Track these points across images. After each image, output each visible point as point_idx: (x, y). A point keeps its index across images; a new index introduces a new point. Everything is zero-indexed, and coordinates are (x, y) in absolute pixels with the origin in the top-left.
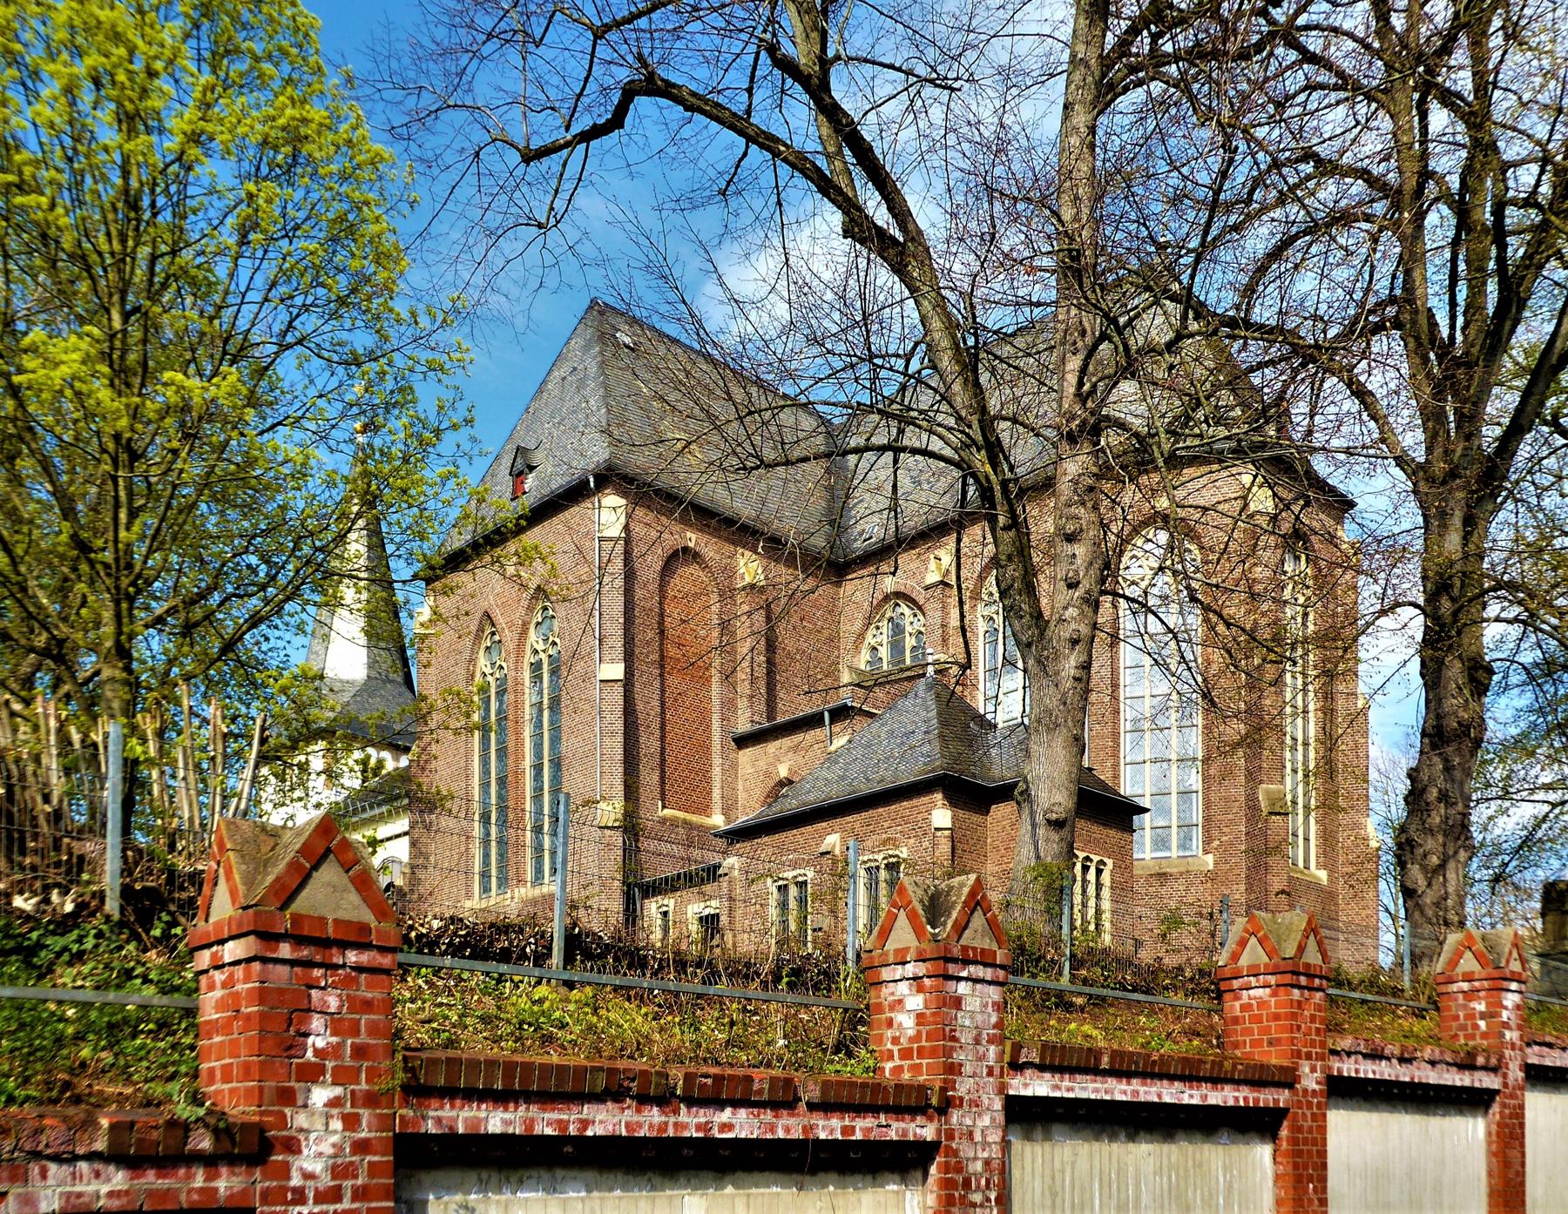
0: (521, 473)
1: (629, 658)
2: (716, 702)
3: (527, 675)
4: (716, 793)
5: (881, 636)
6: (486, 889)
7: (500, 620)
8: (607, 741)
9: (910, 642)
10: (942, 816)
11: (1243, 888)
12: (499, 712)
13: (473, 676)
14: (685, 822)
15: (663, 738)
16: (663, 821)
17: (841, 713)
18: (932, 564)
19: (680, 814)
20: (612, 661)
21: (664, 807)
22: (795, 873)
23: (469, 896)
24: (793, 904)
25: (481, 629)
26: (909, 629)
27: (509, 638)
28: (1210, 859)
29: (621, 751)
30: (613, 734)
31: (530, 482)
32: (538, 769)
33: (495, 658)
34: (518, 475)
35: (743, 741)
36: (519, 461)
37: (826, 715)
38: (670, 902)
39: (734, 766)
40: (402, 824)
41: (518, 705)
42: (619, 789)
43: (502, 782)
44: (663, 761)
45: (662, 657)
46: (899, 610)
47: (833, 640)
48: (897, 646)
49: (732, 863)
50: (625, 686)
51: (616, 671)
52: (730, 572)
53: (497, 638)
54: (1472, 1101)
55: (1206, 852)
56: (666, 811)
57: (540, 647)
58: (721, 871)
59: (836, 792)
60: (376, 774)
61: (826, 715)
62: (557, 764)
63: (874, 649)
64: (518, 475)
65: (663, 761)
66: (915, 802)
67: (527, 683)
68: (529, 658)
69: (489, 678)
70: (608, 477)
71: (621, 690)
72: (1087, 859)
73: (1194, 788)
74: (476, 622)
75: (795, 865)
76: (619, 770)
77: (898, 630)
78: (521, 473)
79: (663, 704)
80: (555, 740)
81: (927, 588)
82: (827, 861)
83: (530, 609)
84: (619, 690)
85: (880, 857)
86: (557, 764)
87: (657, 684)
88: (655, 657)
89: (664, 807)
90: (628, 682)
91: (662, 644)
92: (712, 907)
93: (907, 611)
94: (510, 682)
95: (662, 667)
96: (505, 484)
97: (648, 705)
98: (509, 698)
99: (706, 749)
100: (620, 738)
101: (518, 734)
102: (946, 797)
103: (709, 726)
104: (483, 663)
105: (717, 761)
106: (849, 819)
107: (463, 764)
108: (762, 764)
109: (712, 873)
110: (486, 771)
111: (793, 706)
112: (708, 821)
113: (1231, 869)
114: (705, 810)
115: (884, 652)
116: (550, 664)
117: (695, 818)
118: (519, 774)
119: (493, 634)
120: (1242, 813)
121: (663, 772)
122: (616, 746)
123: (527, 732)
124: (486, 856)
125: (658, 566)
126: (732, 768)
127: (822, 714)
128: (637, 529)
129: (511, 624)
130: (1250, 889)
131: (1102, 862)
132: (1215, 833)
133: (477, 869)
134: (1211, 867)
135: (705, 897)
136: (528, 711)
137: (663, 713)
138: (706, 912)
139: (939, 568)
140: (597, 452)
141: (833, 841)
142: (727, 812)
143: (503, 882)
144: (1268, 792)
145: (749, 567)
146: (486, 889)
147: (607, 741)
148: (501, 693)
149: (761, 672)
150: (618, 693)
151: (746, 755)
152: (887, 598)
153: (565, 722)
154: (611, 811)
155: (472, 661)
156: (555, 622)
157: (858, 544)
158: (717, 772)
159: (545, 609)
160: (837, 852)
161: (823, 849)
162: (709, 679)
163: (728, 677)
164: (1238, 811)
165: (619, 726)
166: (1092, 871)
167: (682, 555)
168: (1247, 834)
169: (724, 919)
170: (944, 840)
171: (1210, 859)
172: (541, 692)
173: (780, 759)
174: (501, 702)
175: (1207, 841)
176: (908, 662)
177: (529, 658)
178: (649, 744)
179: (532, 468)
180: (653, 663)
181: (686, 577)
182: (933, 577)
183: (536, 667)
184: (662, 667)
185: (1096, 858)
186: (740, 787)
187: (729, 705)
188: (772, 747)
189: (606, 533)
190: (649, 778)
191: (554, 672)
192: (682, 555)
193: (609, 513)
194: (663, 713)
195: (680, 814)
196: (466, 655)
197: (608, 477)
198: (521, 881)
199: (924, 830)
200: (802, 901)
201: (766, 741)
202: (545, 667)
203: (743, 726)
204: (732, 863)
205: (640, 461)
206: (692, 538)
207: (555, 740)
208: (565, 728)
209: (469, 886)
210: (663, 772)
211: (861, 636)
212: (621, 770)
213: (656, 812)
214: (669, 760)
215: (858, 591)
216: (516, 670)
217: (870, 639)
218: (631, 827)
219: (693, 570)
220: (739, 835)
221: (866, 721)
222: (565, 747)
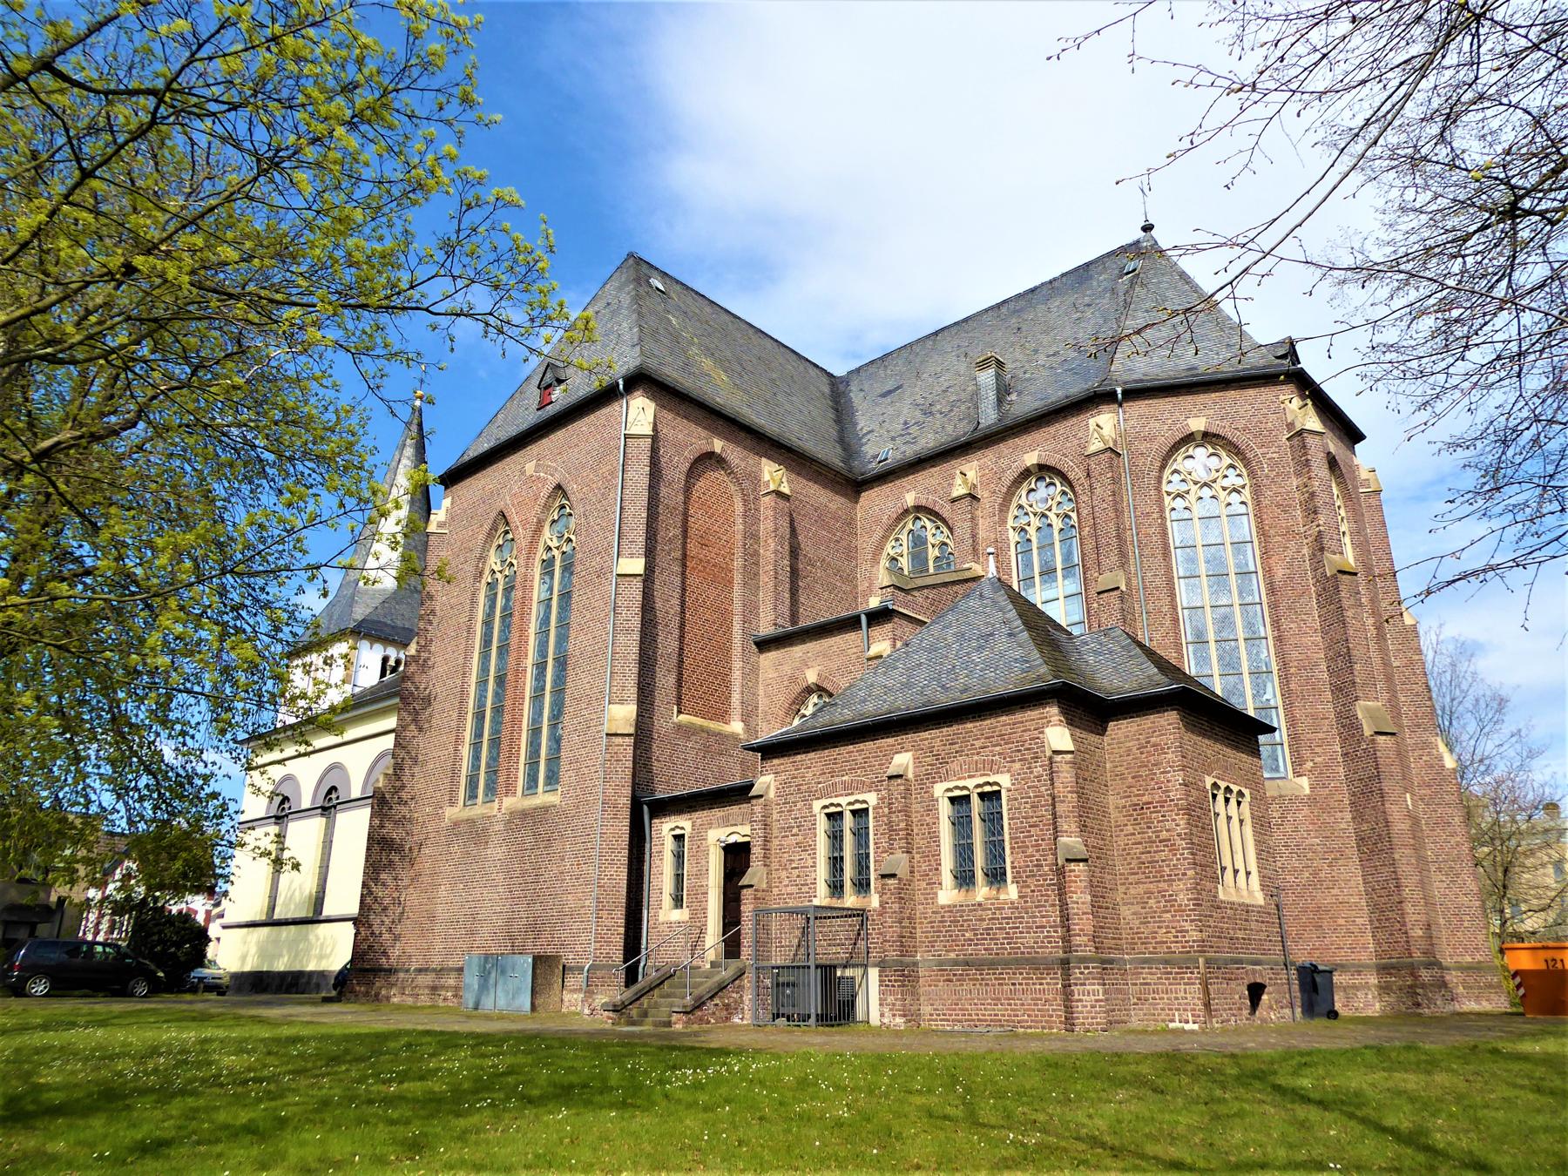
0: (549, 386)
1: (650, 553)
2: (737, 607)
3: (537, 571)
4: (736, 698)
5: (901, 547)
6: (472, 795)
7: (515, 519)
8: (621, 638)
9: (933, 553)
10: (1059, 736)
11: (1349, 816)
12: (504, 609)
13: (481, 573)
14: (702, 729)
15: (682, 637)
16: (679, 726)
17: (880, 616)
18: (959, 480)
19: (698, 721)
20: (632, 556)
21: (679, 712)
22: (851, 799)
23: (452, 803)
24: (848, 840)
25: (494, 528)
26: (931, 540)
27: (522, 535)
28: (1305, 782)
29: (636, 650)
30: (628, 631)
31: (557, 393)
32: (541, 667)
33: (506, 555)
34: (546, 388)
35: (764, 645)
36: (549, 375)
37: (863, 618)
38: (684, 823)
39: (755, 670)
40: (391, 722)
41: (526, 601)
42: (632, 691)
43: (501, 680)
44: (681, 662)
45: (685, 556)
46: (919, 524)
47: (851, 553)
48: (919, 558)
49: (767, 781)
50: (644, 581)
51: (637, 565)
52: (755, 479)
53: (510, 536)
54: (1060, 872)
55: (1298, 774)
56: (682, 717)
57: (555, 543)
58: (753, 792)
59: (904, 703)
60: (394, 670)
61: (863, 618)
62: (562, 663)
63: (894, 559)
64: (546, 388)
65: (681, 662)
66: (1019, 716)
67: (537, 577)
68: (541, 554)
69: (498, 575)
70: (639, 380)
71: (640, 585)
72: (1228, 790)
73: (1272, 703)
74: (490, 522)
75: (849, 789)
76: (633, 670)
77: (919, 542)
78: (549, 386)
79: (683, 603)
80: (562, 638)
81: (954, 501)
82: (898, 787)
83: (547, 507)
84: (638, 585)
85: (970, 783)
86: (562, 663)
87: (677, 581)
88: (678, 554)
89: (679, 712)
90: (648, 577)
91: (684, 544)
92: (739, 833)
93: (928, 524)
94: (519, 579)
95: (684, 566)
96: (533, 394)
97: (668, 605)
98: (517, 594)
99: (726, 651)
100: (636, 636)
101: (523, 630)
102: (1064, 712)
103: (730, 628)
104: (493, 561)
105: (737, 664)
106: (925, 735)
107: (461, 661)
108: (787, 669)
109: (740, 794)
110: (484, 669)
111: (816, 611)
112: (727, 729)
113: (1331, 794)
114: (723, 715)
115: (904, 562)
116: (563, 560)
117: (713, 725)
118: (520, 672)
119: (507, 532)
120: (1335, 731)
121: (680, 674)
122: (630, 645)
123: (533, 627)
124: (476, 757)
125: (686, 466)
126: (752, 673)
127: (858, 617)
128: (664, 431)
129: (525, 523)
130: (1359, 817)
131: (1240, 794)
132: (1306, 753)
133: (464, 772)
134: (1307, 791)
135: (726, 822)
136: (535, 610)
137: (683, 612)
138: (732, 840)
139: (965, 482)
140: (624, 362)
141: (903, 760)
142: (746, 719)
143: (491, 789)
144: (1367, 709)
145: (772, 473)
146: (472, 795)
147: (621, 638)
148: (509, 590)
149: (785, 577)
150: (635, 591)
151: (769, 659)
152: (906, 512)
153: (575, 619)
154: (623, 714)
155: (482, 558)
156: (572, 520)
157: (874, 465)
158: (737, 675)
159: (563, 507)
160: (910, 775)
161: (892, 771)
162: (731, 582)
163: (751, 575)
164: (1329, 729)
165: (636, 622)
166: (1233, 802)
167: (708, 460)
168: (1345, 755)
169: (756, 851)
170: (1066, 767)
171: (1305, 782)
172: (551, 589)
173: (811, 662)
174: (508, 600)
175: (1298, 762)
176: (931, 571)
177: (541, 554)
178: (667, 644)
179: (560, 381)
180: (674, 559)
181: (711, 480)
182: (959, 490)
183: (548, 565)
184: (684, 566)
185: (1235, 788)
186: (761, 692)
187: (751, 611)
188: (798, 651)
189: (633, 431)
190: (665, 681)
191: (568, 568)
192: (708, 460)
193: (640, 412)
194: (683, 612)
195: (698, 721)
196: (477, 553)
197: (639, 380)
198: (510, 790)
199: (1032, 751)
200: (861, 835)
201: (791, 645)
202: (558, 563)
203: (766, 629)
204: (767, 781)
205: (671, 372)
206: (718, 445)
207: (562, 638)
208: (574, 625)
209: (453, 793)
210: (680, 674)
211: (880, 547)
212: (635, 670)
213: (670, 718)
214: (687, 662)
215: (878, 503)
216: (527, 566)
217: (889, 549)
218: (643, 735)
219: (720, 475)
220: (771, 750)
221: (908, 628)
222: (572, 647)
